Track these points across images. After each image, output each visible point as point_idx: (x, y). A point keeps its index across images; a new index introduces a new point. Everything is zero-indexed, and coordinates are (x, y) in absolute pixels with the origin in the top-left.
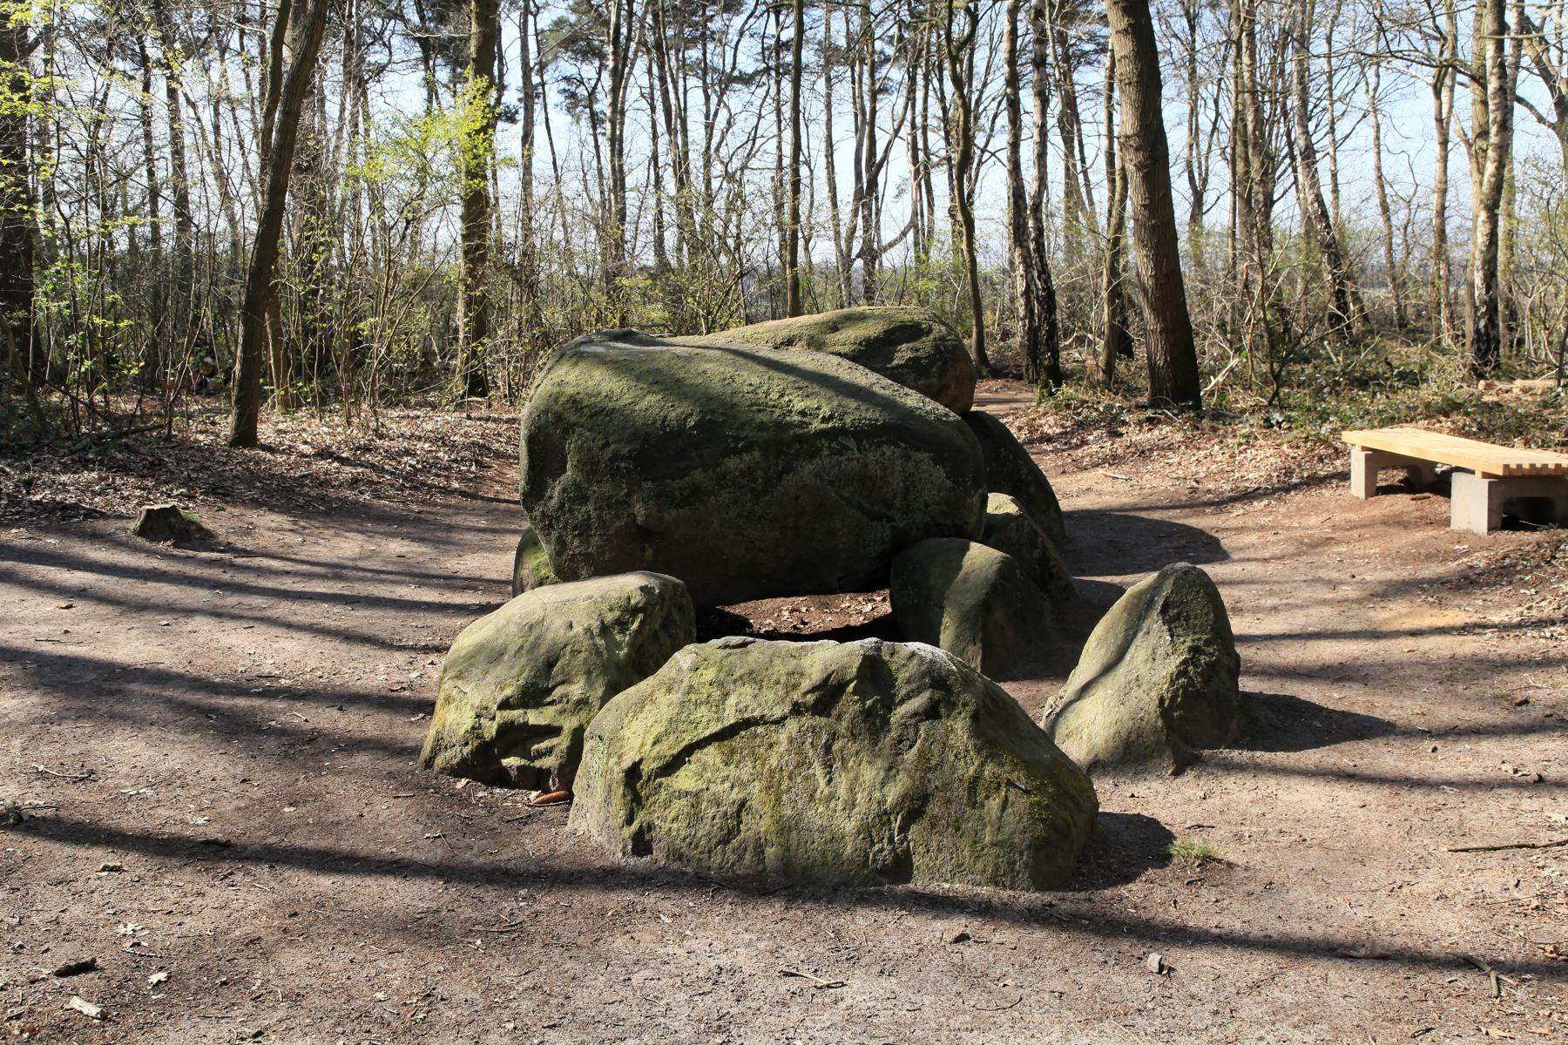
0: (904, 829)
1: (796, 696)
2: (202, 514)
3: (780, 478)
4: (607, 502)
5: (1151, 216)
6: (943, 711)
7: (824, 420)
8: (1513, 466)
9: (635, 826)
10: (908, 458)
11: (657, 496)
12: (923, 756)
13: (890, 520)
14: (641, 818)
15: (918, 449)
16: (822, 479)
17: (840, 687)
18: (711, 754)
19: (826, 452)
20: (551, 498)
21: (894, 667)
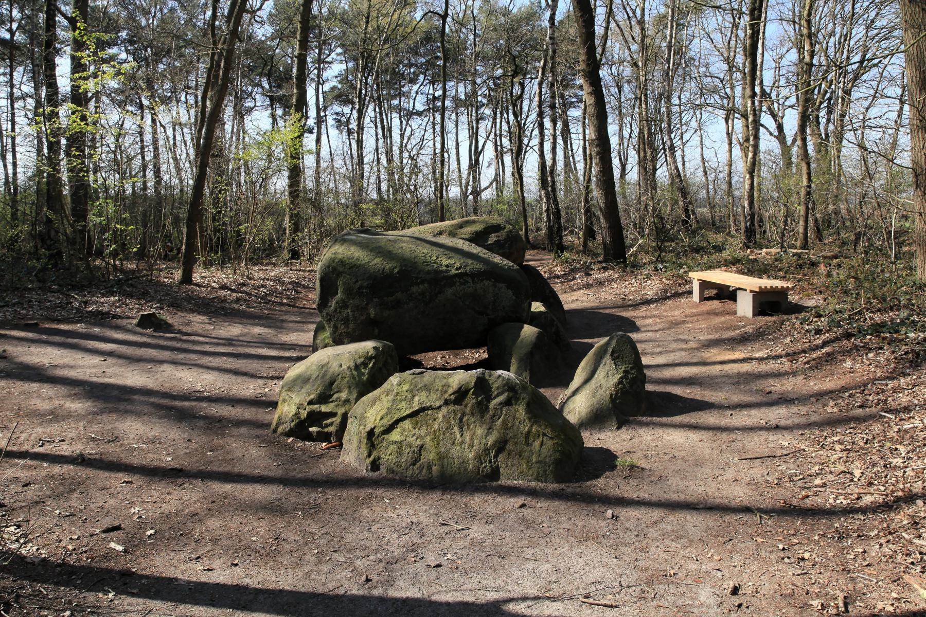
0: (496, 456)
1: (446, 396)
2: (166, 316)
5: (603, 176)
7: (457, 269)
12: (505, 423)
14: (375, 454)
17: (467, 391)
18: (407, 424)
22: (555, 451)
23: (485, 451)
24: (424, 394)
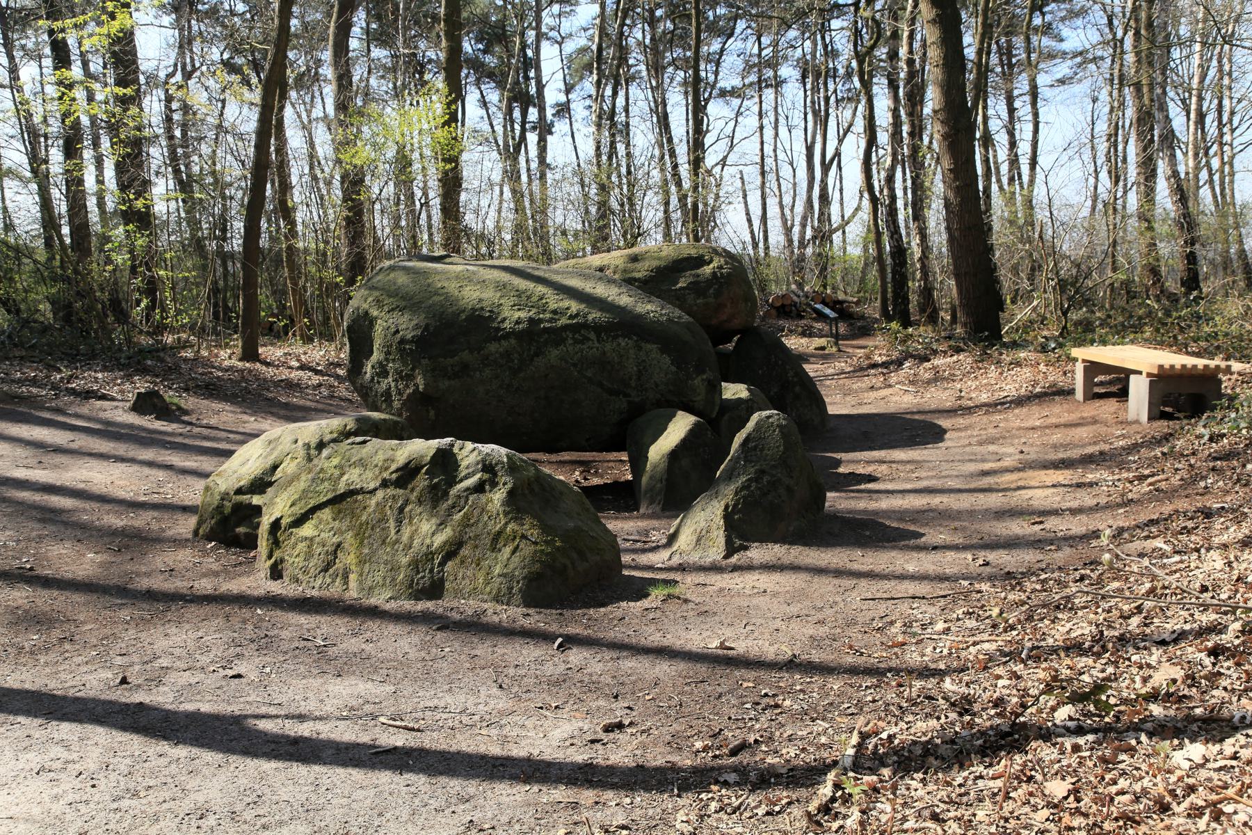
0: (443, 564)
1: (386, 475)
2: (170, 396)
3: (532, 360)
4: (400, 377)
5: (956, 179)
6: (487, 487)
7: (571, 317)
8: (1167, 366)
9: (273, 560)
10: (640, 349)
11: (433, 370)
12: (467, 517)
13: (626, 395)
14: (277, 554)
15: (648, 341)
16: (567, 362)
17: (417, 469)
18: (326, 514)
19: (570, 341)
21: (459, 458)
22: (533, 561)
23: (426, 555)
24: (357, 471)
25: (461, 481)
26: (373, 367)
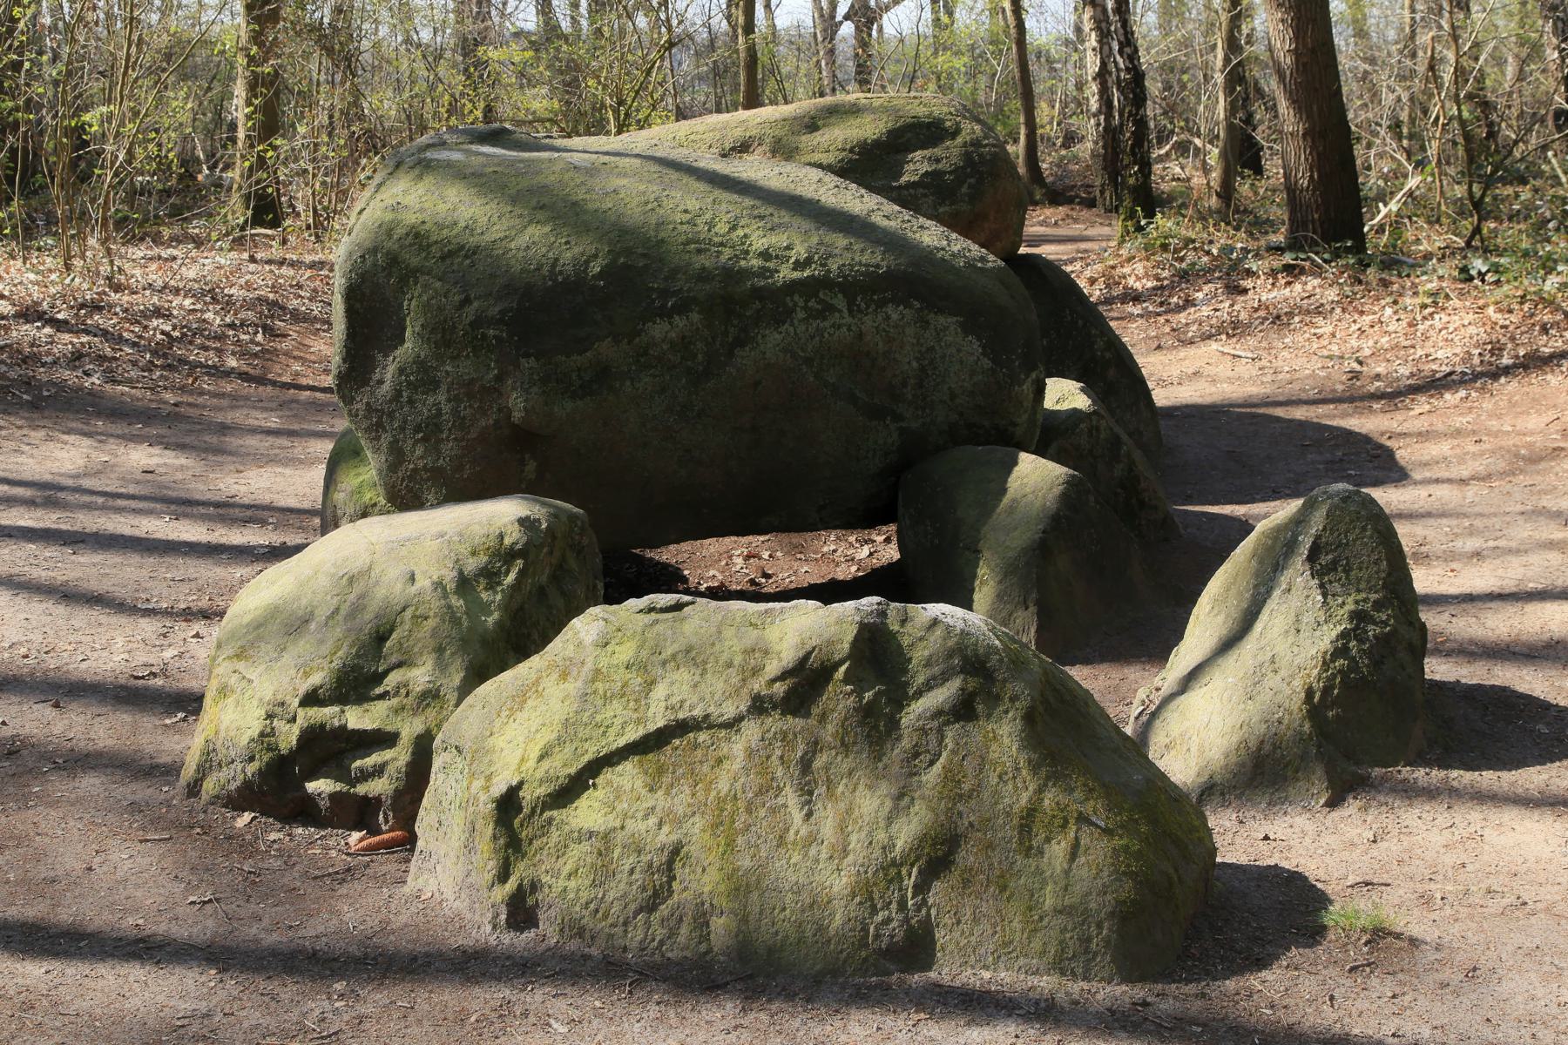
0: (921, 888)
1: (758, 685)
6: (980, 708)
7: (798, 265)
9: (511, 885)
10: (925, 324)
12: (951, 778)
15: (940, 311)
18: (627, 775)
19: (801, 315)
20: (381, 382)
21: (906, 641)
23: (884, 868)
25: (919, 694)
26: (401, 371)
